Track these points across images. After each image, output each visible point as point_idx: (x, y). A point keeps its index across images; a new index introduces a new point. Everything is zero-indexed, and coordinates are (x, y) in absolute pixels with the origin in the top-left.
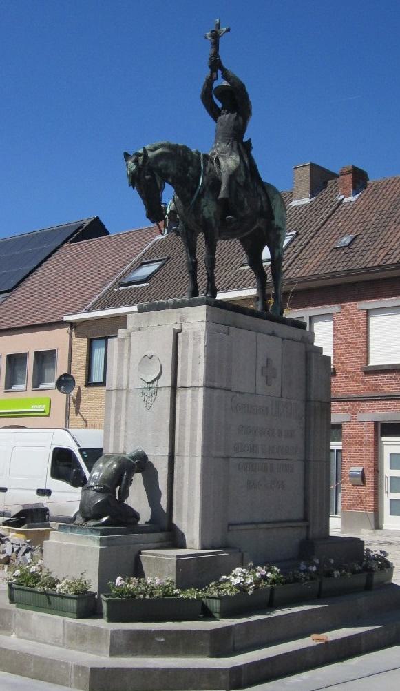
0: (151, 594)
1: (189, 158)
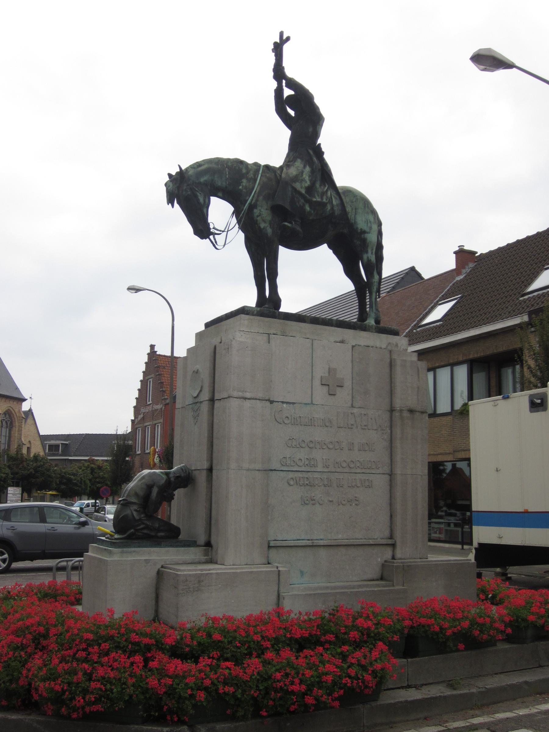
0: (40, 593)
1: (244, 171)
